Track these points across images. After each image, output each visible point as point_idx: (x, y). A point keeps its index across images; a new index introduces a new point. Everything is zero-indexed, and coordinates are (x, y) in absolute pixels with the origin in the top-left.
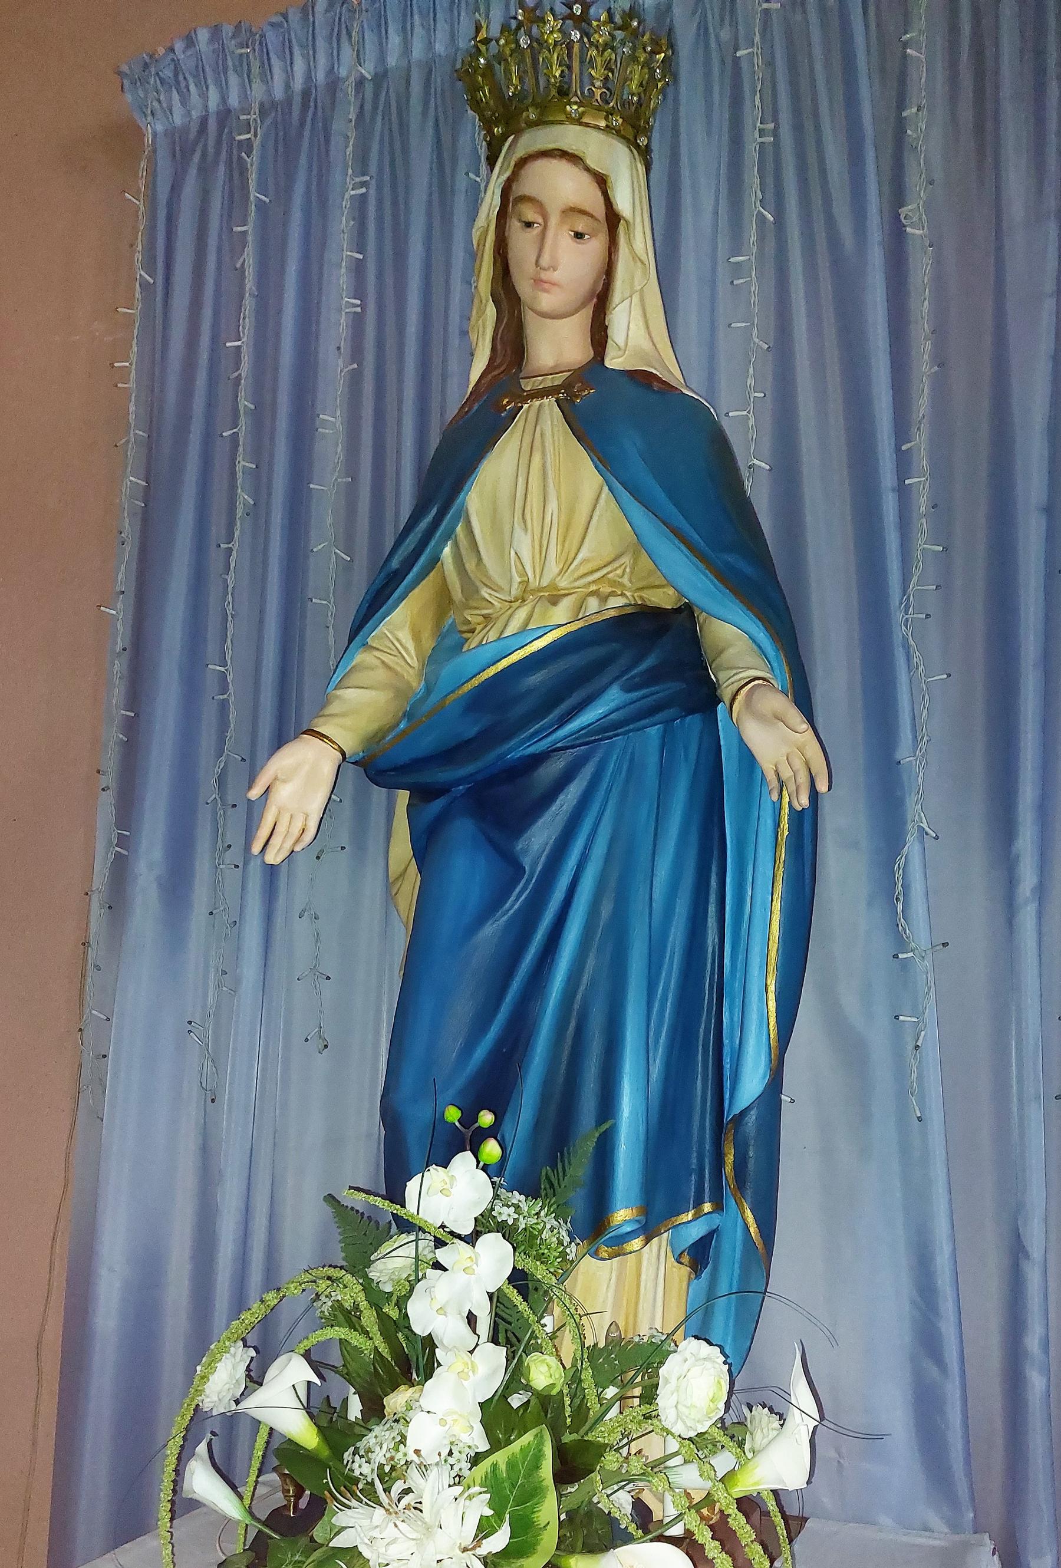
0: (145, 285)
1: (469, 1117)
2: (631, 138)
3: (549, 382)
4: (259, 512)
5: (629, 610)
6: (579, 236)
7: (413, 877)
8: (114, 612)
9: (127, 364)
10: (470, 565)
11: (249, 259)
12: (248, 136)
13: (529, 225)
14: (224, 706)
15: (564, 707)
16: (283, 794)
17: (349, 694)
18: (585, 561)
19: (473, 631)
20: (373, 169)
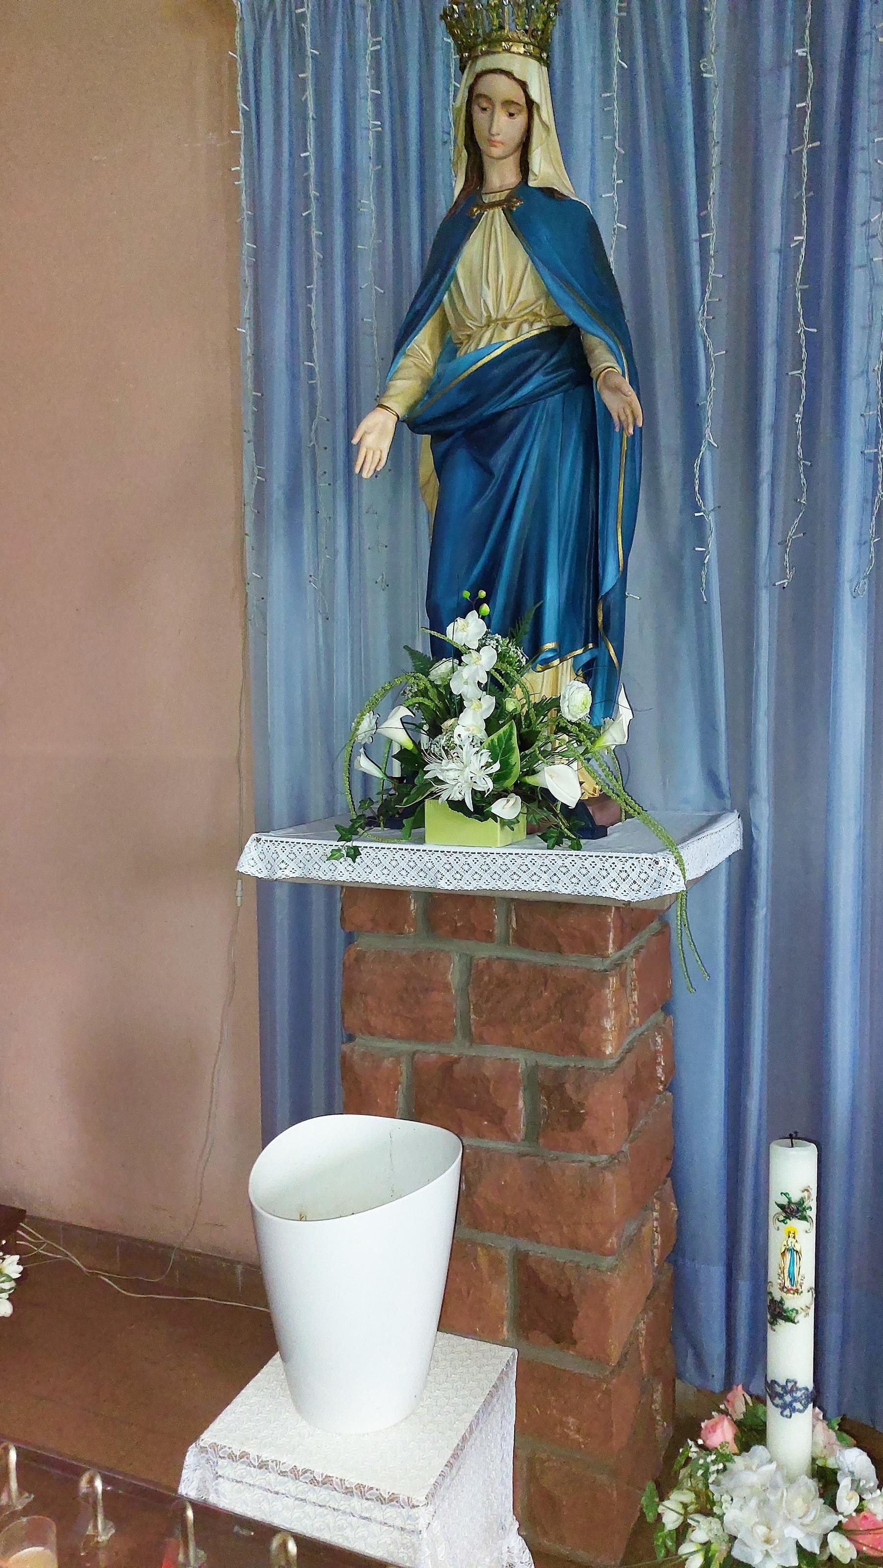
0: (245, 113)
1: (474, 595)
2: (538, 55)
3: (498, 197)
4: (326, 262)
5: (545, 330)
6: (511, 115)
7: (435, 482)
8: (244, 331)
9: (238, 168)
10: (459, 307)
11: (310, 93)
12: (302, 10)
13: (484, 109)
14: (312, 388)
15: (511, 387)
16: (369, 440)
17: (399, 383)
18: (520, 303)
19: (461, 343)
20: (384, 33)
